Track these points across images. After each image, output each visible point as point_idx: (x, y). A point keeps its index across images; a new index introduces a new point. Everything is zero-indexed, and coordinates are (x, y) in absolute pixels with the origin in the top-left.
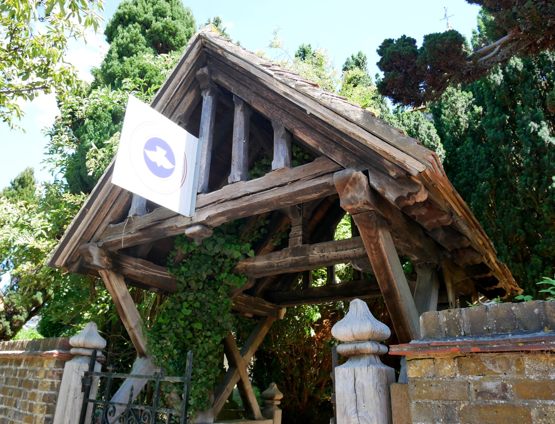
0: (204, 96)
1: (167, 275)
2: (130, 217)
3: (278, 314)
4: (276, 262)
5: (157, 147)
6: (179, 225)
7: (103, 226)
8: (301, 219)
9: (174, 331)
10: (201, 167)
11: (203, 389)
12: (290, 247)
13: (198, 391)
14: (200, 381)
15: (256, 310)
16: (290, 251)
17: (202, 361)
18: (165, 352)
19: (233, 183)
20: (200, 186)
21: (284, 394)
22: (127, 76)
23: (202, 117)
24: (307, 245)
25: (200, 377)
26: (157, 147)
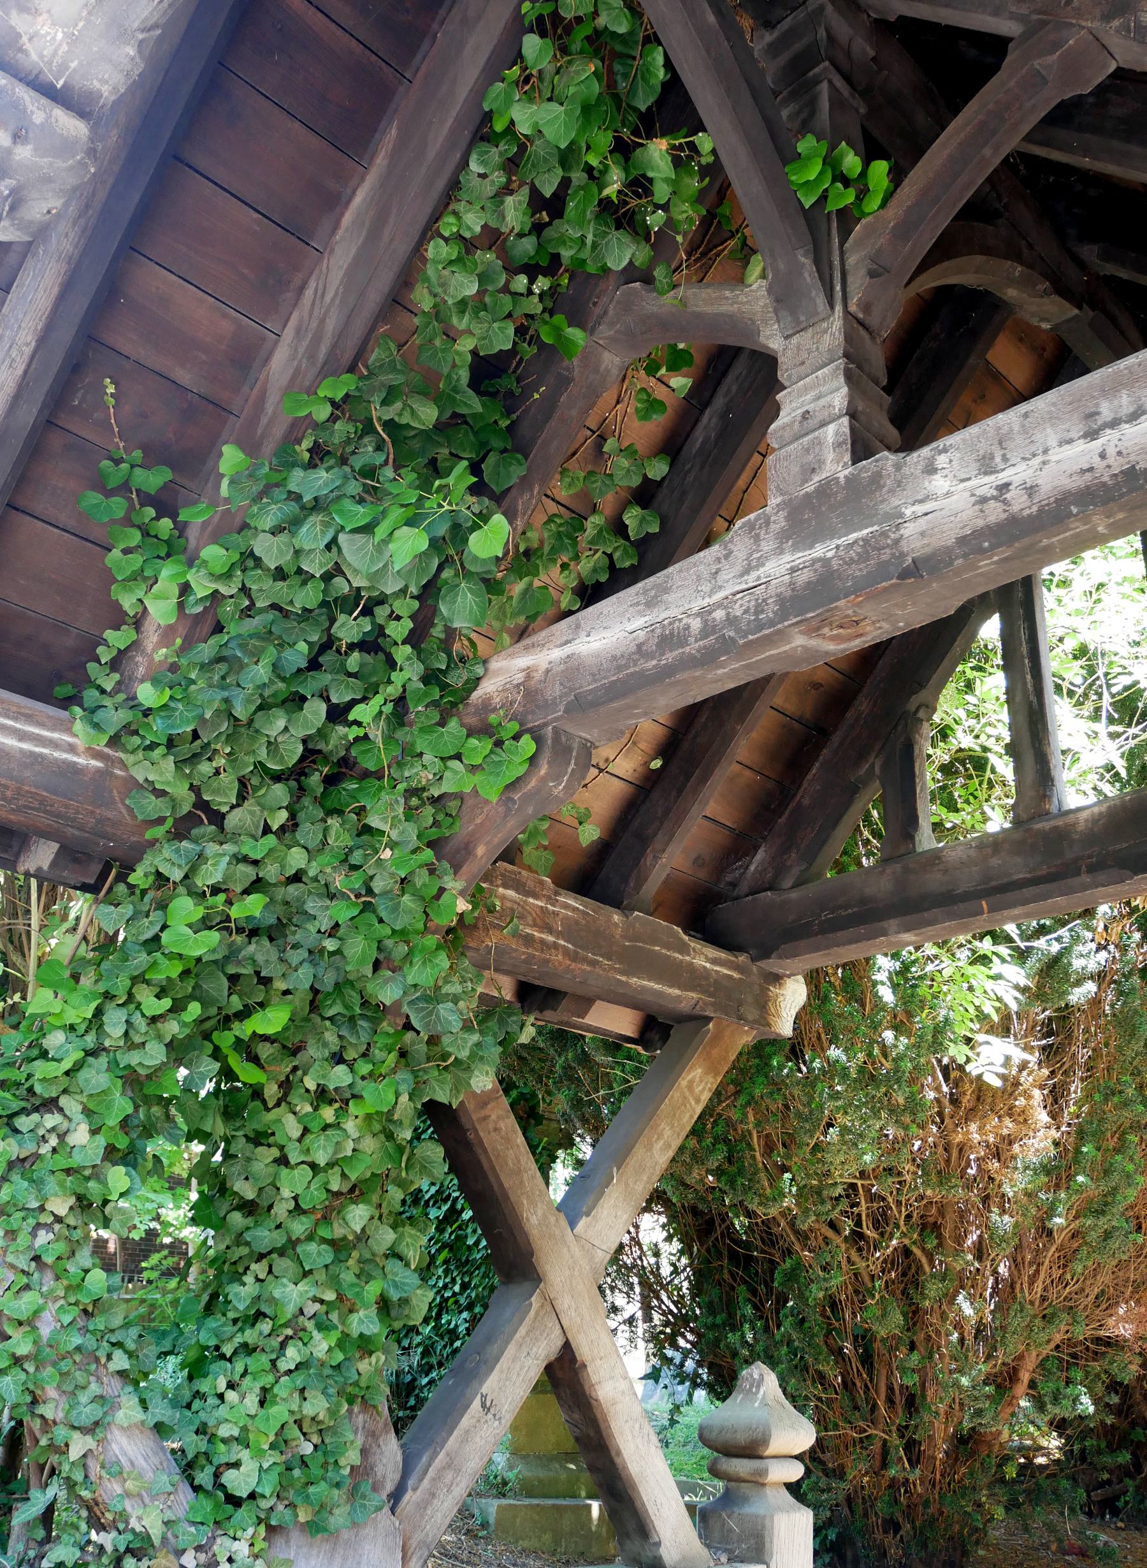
1: (72, 749)
3: (764, 1006)
4: (697, 605)
8: (836, 322)
9: (113, 1065)
11: (317, 1406)
12: (774, 501)
13: (279, 1412)
14: (293, 1354)
15: (634, 981)
16: (780, 521)
17: (310, 1238)
18: (51, 1184)
21: (821, 1422)
24: (887, 460)
25: (300, 1335)
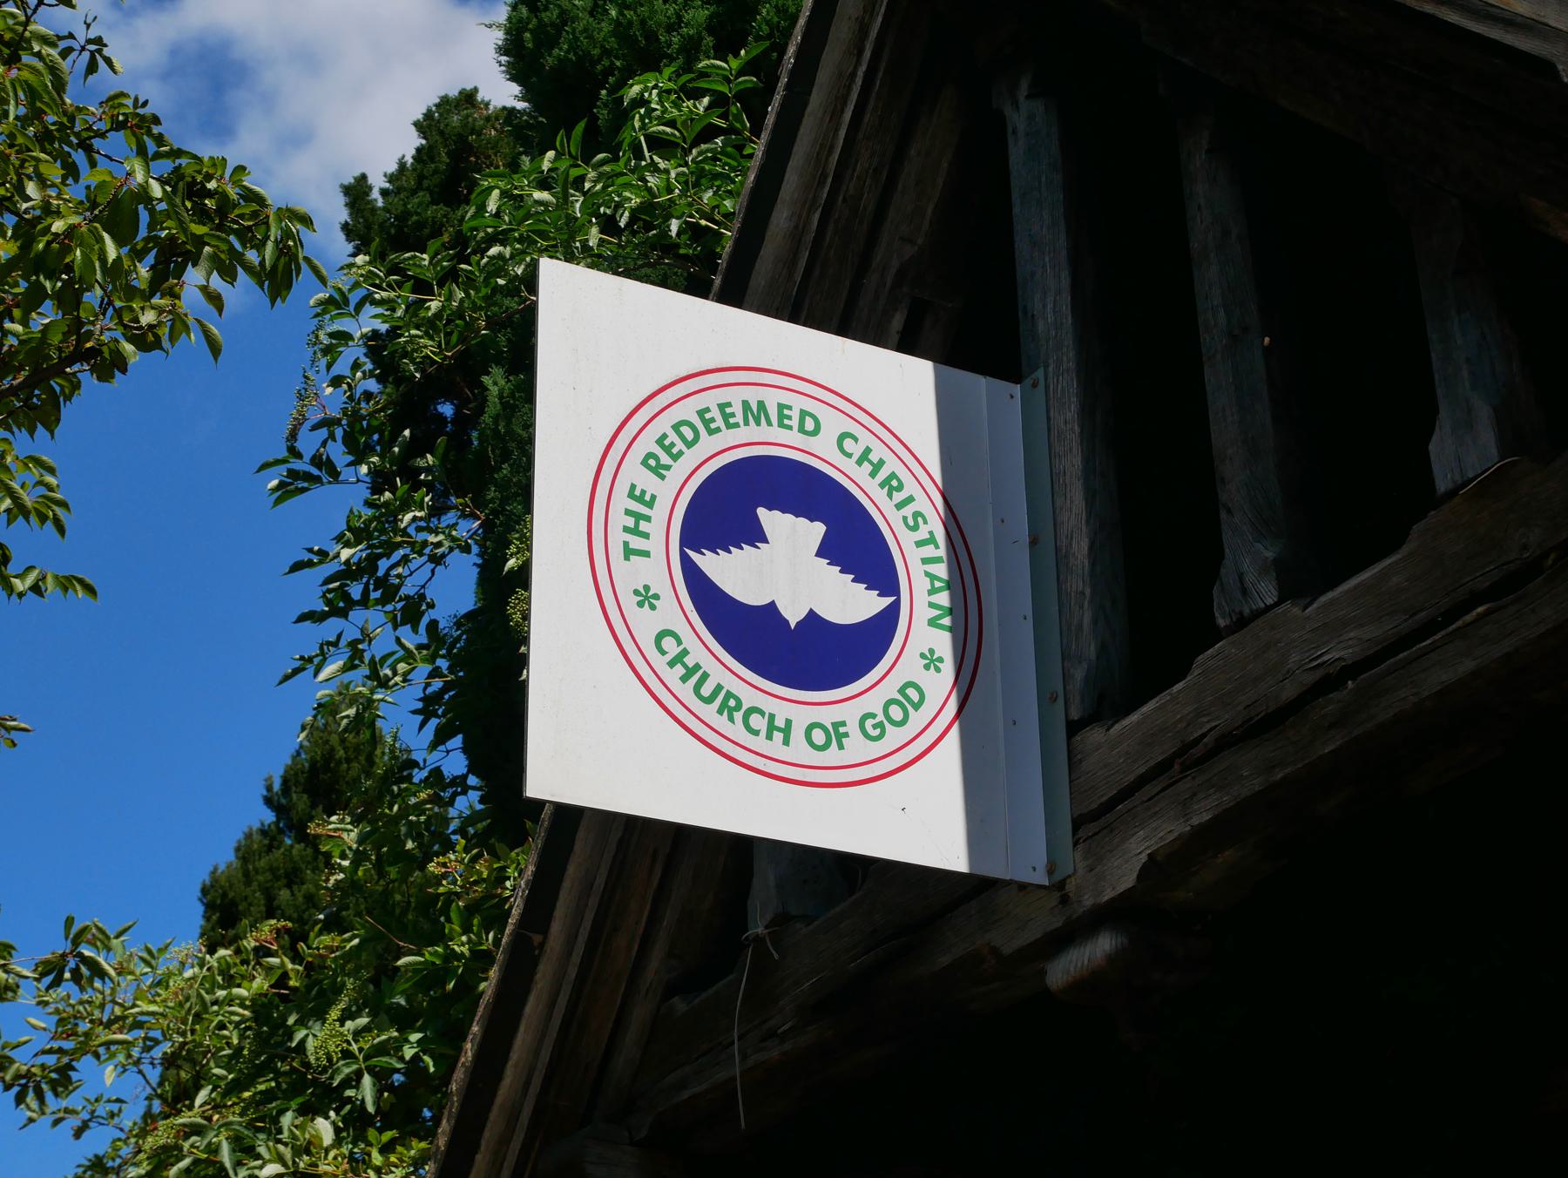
0: (1008, 111)
2: (758, 939)
5: (768, 518)
6: (1010, 940)
7: (641, 1013)
10: (1062, 557)
19: (1241, 623)
20: (1079, 674)
22: (648, 59)
23: (1022, 246)
26: (768, 518)
